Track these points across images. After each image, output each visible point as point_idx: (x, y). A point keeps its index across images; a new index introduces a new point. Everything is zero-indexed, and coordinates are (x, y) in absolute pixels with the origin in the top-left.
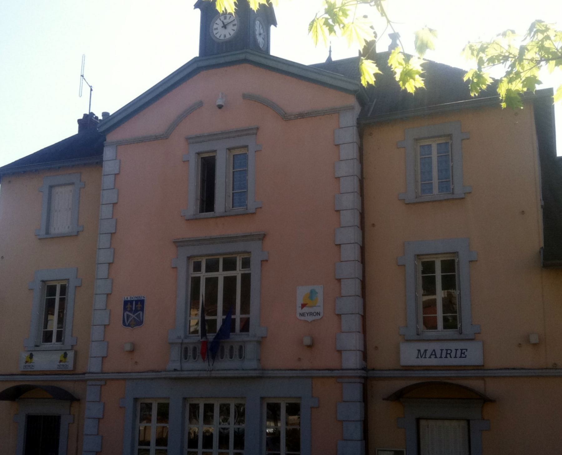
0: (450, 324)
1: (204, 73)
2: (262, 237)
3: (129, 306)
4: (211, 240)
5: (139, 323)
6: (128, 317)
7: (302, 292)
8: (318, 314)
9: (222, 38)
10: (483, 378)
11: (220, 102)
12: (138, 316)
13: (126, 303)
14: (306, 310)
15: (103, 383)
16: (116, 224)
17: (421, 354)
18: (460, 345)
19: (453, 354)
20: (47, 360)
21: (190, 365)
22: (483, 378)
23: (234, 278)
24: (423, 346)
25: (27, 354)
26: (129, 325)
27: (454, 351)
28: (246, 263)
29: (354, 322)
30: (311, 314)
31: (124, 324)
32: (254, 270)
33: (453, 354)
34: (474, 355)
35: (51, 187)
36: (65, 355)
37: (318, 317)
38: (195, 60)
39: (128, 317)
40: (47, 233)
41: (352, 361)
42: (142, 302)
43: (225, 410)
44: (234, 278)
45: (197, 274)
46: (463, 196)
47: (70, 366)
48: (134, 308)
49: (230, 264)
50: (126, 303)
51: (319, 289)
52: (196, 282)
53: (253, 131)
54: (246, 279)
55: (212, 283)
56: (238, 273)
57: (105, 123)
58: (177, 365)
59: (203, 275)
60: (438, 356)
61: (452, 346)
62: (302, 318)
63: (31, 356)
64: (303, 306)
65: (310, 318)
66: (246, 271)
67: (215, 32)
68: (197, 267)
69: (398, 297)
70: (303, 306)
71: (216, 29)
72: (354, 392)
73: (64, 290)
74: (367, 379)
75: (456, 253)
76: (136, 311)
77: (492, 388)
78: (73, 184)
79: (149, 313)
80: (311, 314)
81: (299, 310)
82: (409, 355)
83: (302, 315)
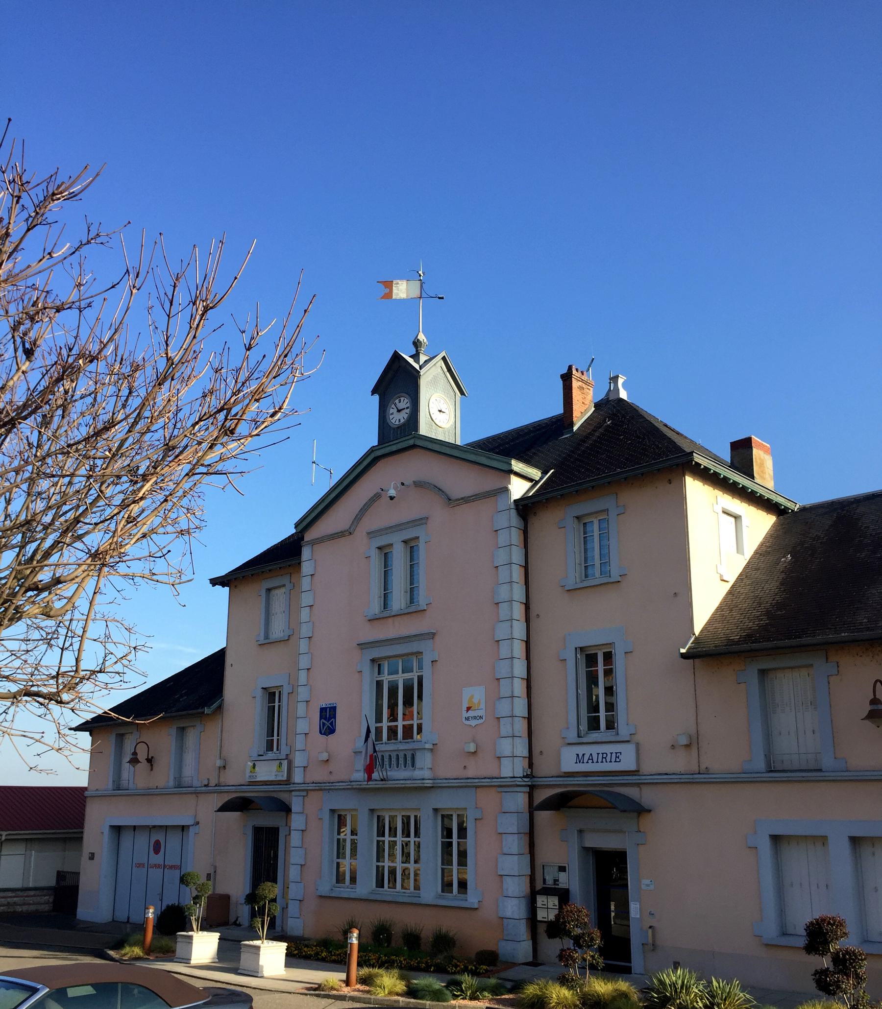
1: (381, 464)
2: (432, 635)
3: (324, 714)
6: (324, 724)
8: (481, 717)
9: (397, 423)
10: (638, 785)
12: (331, 724)
14: (471, 713)
15: (304, 793)
17: (579, 759)
19: (608, 759)
20: (267, 772)
22: (638, 785)
24: (580, 750)
25: (250, 764)
26: (324, 734)
27: (609, 755)
30: (475, 718)
31: (321, 733)
33: (608, 759)
35: (269, 590)
36: (281, 764)
37: (481, 721)
38: (372, 450)
39: (324, 724)
40: (267, 637)
41: (519, 768)
46: (619, 579)
47: (285, 778)
53: (422, 521)
57: (587, 437)
60: (595, 760)
62: (467, 722)
64: (468, 709)
67: (391, 417)
70: (468, 709)
71: (392, 414)
73: (608, 657)
76: (330, 718)
77: (646, 797)
78: (284, 586)
80: (475, 718)
81: (465, 714)
83: (467, 719)
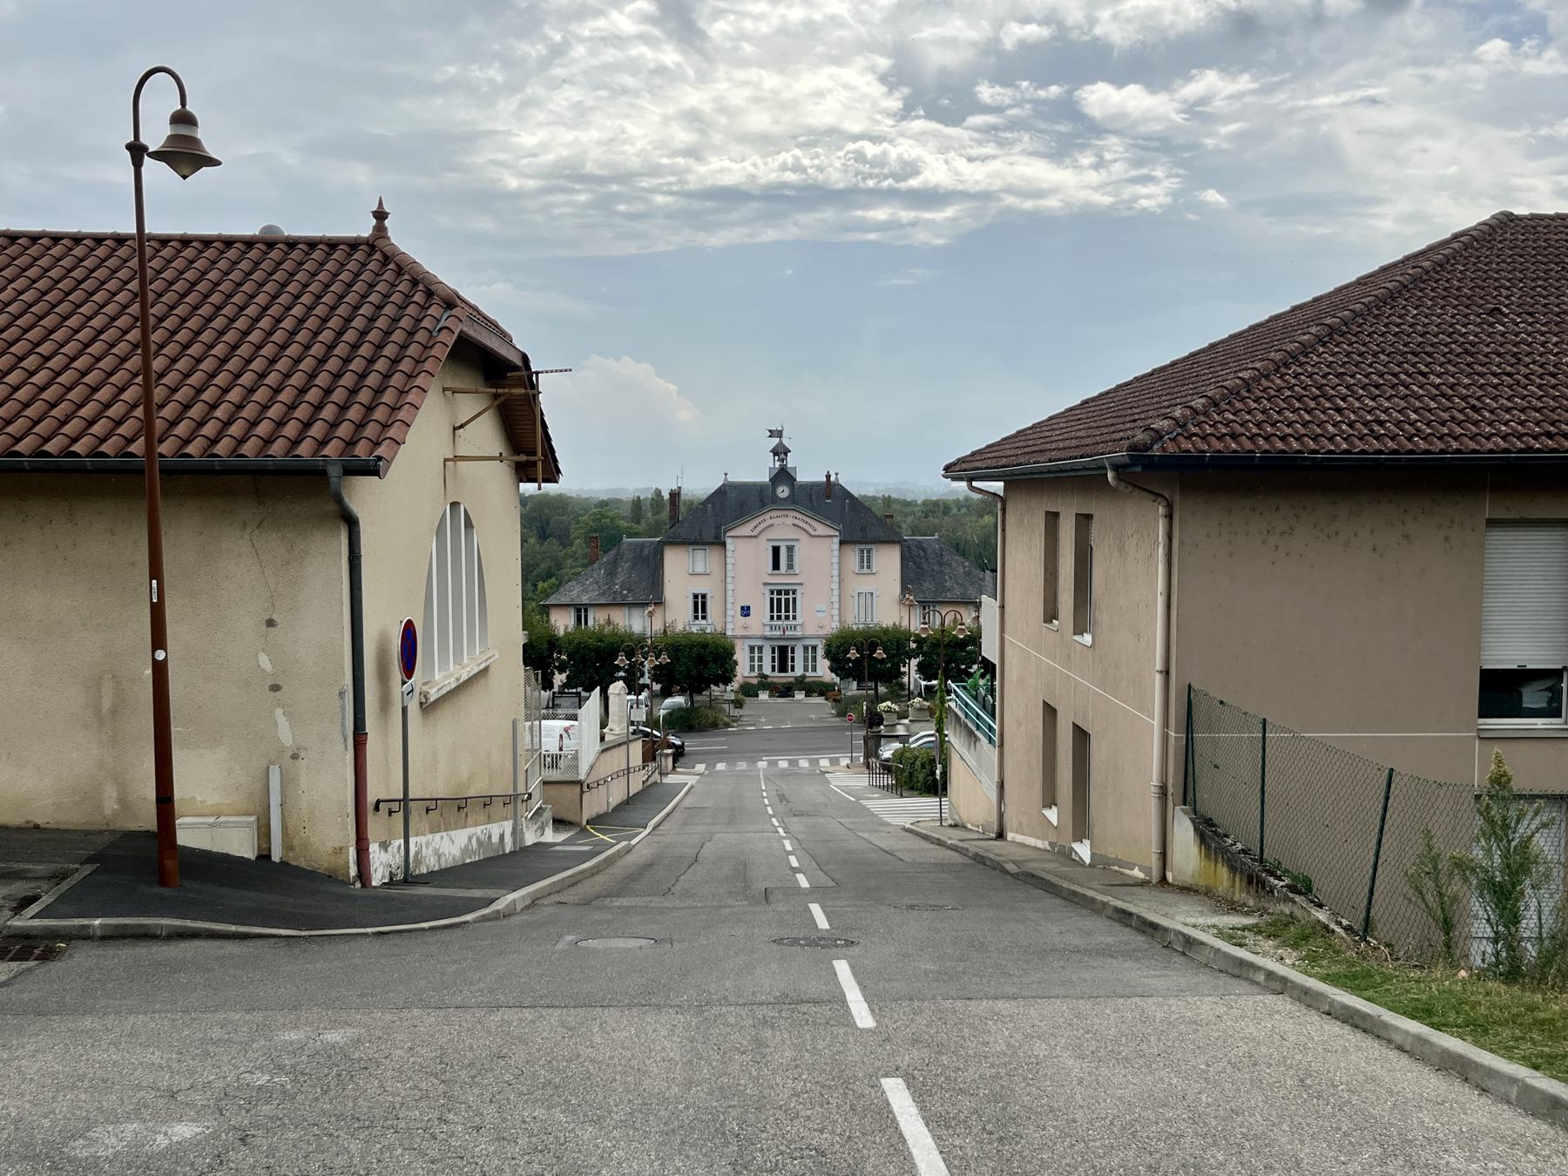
2: (1050, 712)
55: (779, 601)
56: (791, 596)
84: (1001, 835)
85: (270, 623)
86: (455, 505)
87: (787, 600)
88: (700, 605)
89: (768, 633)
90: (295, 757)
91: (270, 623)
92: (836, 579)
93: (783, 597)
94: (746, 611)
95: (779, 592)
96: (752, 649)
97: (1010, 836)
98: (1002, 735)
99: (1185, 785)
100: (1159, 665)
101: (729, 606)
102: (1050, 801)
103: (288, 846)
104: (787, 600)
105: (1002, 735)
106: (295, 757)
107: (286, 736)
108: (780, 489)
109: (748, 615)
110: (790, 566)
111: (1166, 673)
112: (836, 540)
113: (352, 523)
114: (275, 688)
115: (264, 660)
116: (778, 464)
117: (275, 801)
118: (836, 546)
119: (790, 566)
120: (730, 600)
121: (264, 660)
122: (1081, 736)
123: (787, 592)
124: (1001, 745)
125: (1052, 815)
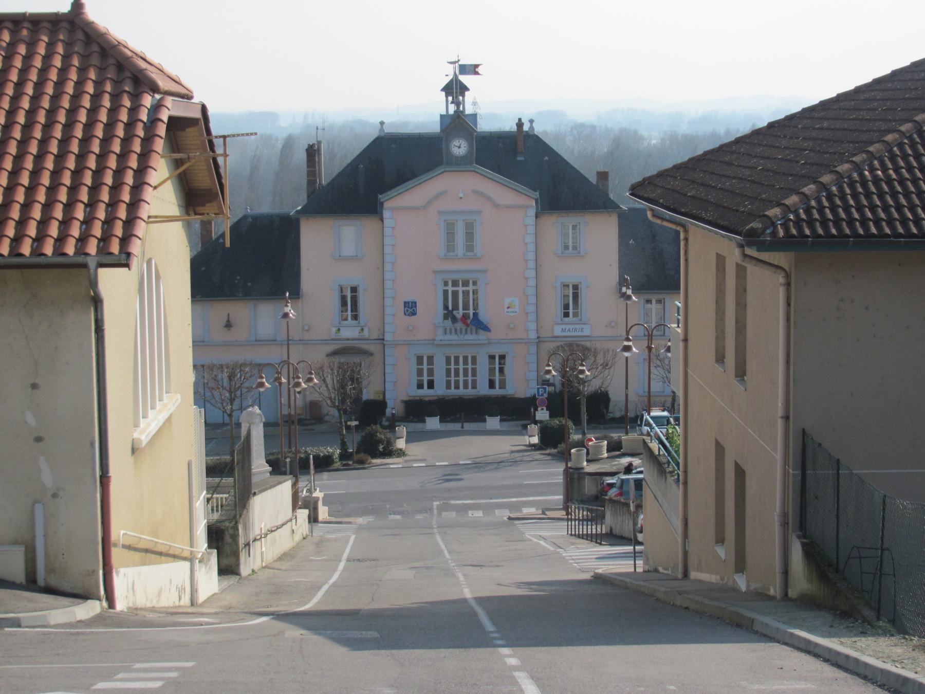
0: (576, 315)
4: (458, 272)
5: (414, 314)
7: (507, 301)
11: (461, 195)
13: (405, 303)
16: (838, 526)
17: (563, 330)
18: (582, 326)
21: (448, 337)
23: (468, 292)
24: (564, 327)
28: (475, 283)
29: (532, 317)
32: (481, 287)
34: (587, 331)
41: (533, 335)
42: (415, 303)
43: (465, 358)
44: (468, 292)
45: (446, 288)
48: (411, 308)
49: (466, 283)
50: (405, 303)
51: (517, 300)
52: (446, 293)
53: (479, 212)
54: (475, 292)
55: (455, 294)
56: (471, 288)
58: (441, 338)
59: (450, 289)
61: (577, 326)
63: (339, 330)
65: (512, 314)
66: (475, 288)
68: (446, 284)
69: (553, 307)
72: (533, 349)
74: (540, 340)
75: (319, 143)
79: (419, 309)
81: (506, 310)
82: (558, 331)
84: (686, 575)
85: (34, 386)
86: (149, 262)
87: (466, 293)
88: (350, 302)
89: (440, 336)
90: (55, 496)
91: (34, 386)
92: (532, 264)
93: (461, 289)
94: (411, 308)
95: (455, 283)
96: (420, 360)
97: (694, 575)
98: (686, 472)
99: (801, 517)
100: (780, 412)
101: (388, 302)
102: (720, 539)
103: (50, 570)
104: (466, 293)
105: (686, 472)
106: (55, 496)
107: (47, 478)
108: (456, 143)
109: (414, 314)
110: (470, 248)
111: (786, 418)
112: (532, 212)
113: (97, 302)
114: (39, 439)
115: (30, 418)
116: (452, 109)
117: (40, 531)
118: (531, 220)
119: (470, 248)
120: (388, 293)
121: (30, 418)
122: (740, 473)
123: (466, 283)
124: (685, 483)
125: (721, 551)
